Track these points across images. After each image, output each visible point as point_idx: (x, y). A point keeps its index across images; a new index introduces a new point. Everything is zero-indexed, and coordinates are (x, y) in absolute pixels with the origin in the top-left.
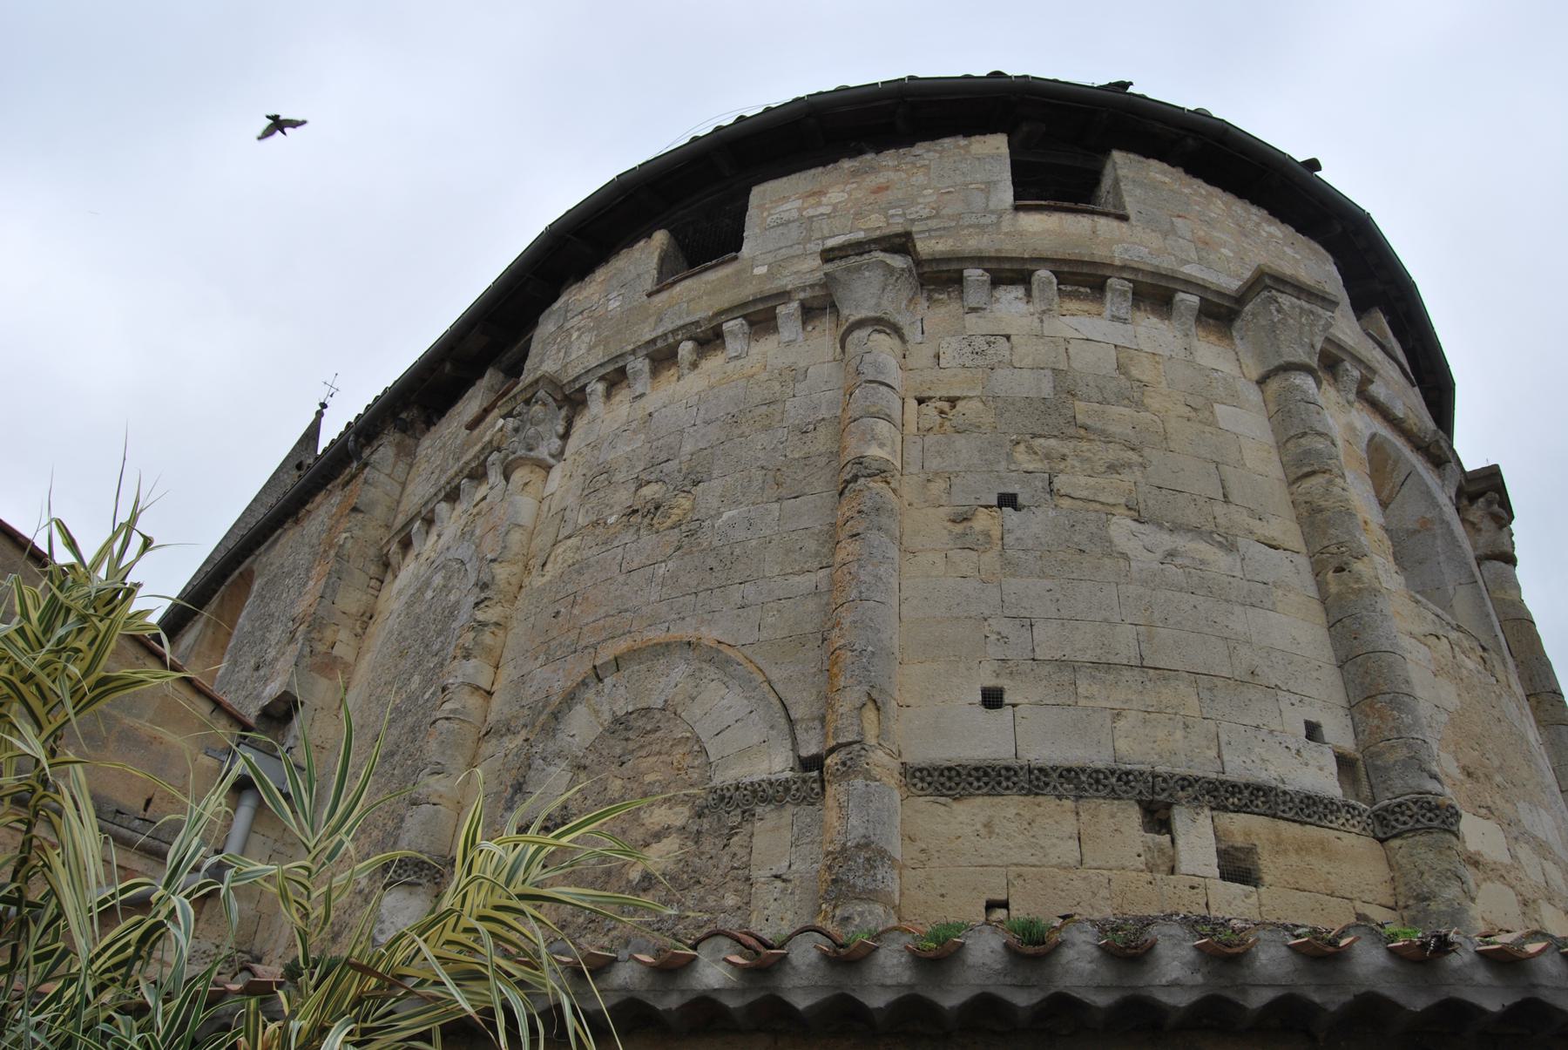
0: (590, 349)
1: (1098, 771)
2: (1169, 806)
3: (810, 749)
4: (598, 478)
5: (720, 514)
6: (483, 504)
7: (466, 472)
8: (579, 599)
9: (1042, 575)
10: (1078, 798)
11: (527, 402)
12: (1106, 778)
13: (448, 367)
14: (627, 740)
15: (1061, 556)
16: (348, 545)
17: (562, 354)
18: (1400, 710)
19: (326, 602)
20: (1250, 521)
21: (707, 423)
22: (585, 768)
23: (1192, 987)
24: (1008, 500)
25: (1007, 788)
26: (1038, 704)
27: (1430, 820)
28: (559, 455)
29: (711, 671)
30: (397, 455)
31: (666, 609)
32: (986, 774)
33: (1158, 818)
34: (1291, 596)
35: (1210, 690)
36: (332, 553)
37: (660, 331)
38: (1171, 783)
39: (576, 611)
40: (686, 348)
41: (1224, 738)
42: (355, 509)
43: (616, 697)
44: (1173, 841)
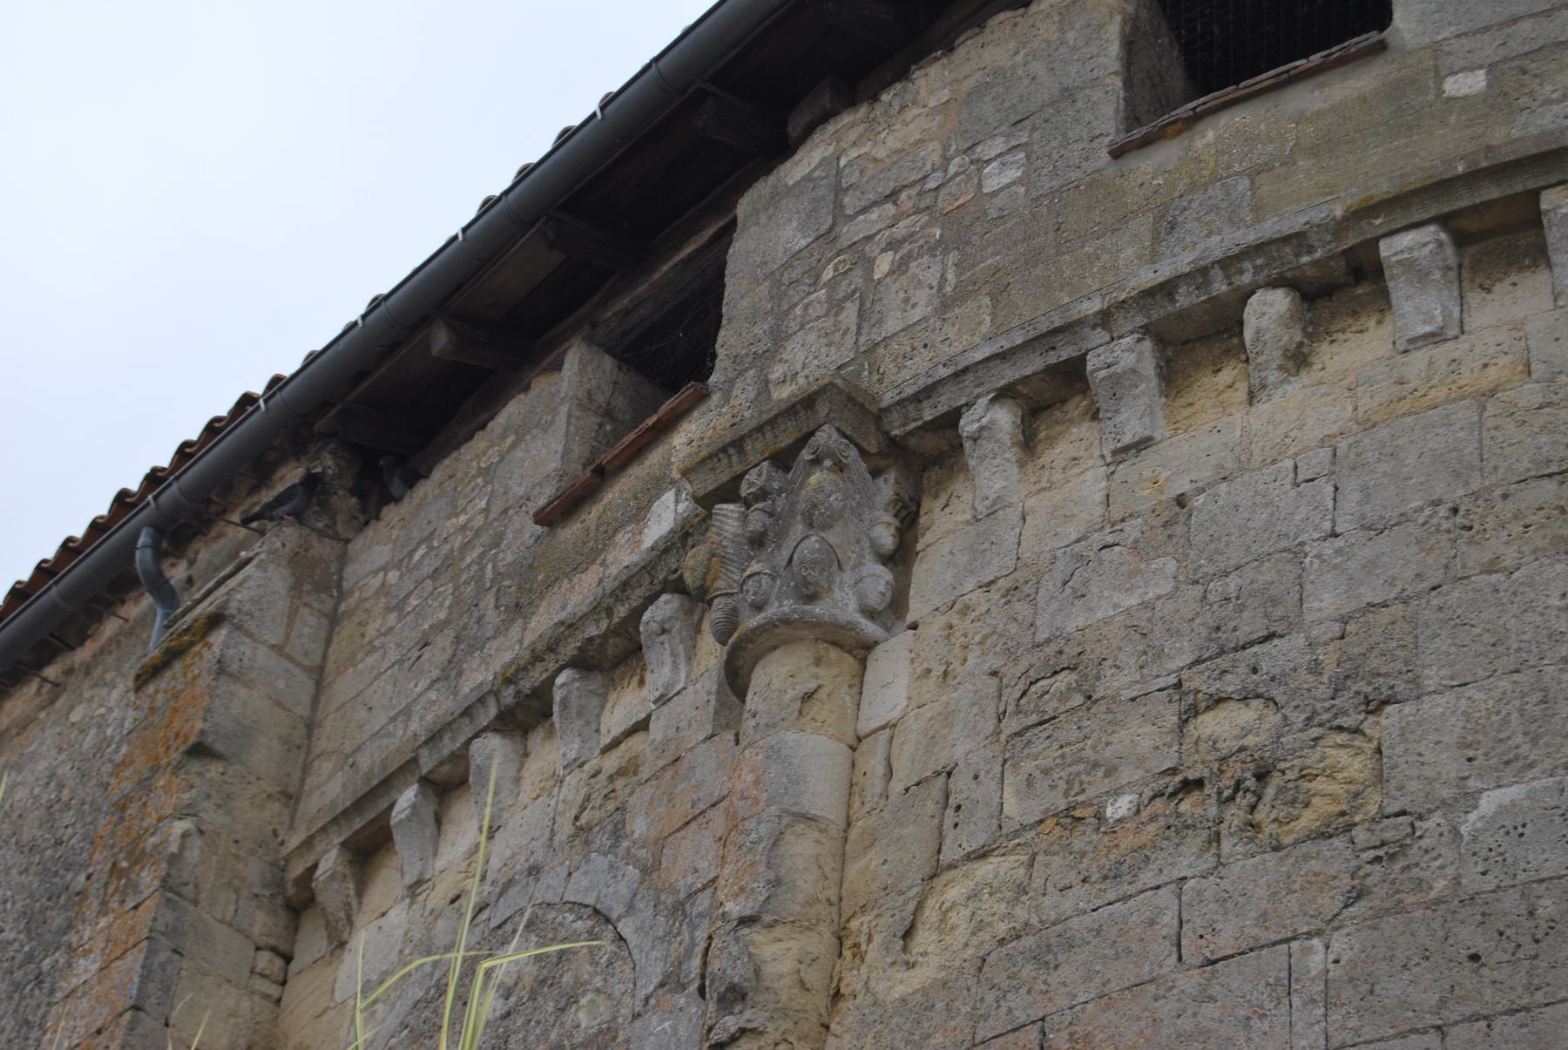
0: (945, 305)
4: (1047, 689)
5: (1470, 799)
6: (636, 743)
7: (569, 649)
11: (783, 460)
13: (441, 339)
16: (193, 854)
17: (850, 315)
19: (149, 1022)
21: (1374, 529)
28: (895, 607)
30: (296, 589)
36: (148, 878)
37: (1184, 261)
40: (1269, 311)
42: (200, 751)
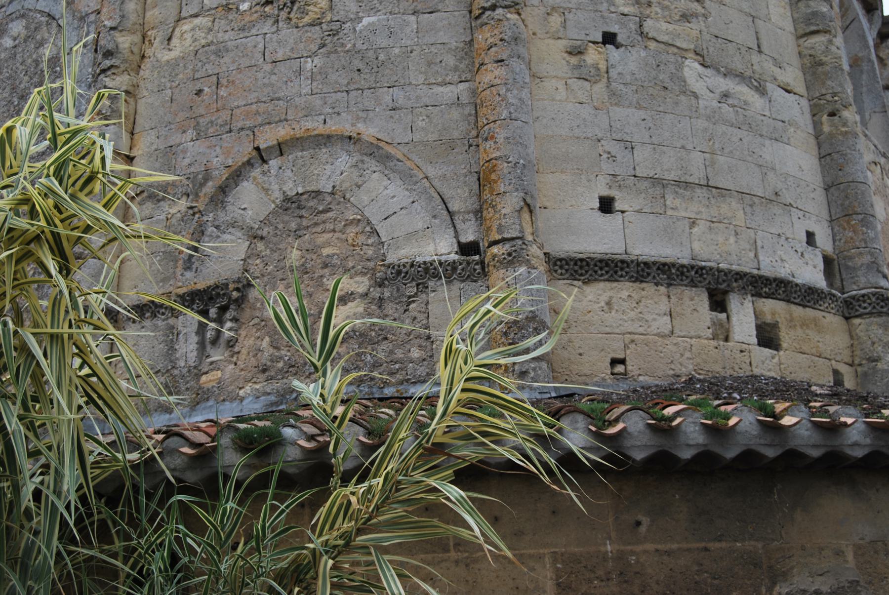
1: (683, 266)
2: (725, 293)
3: (468, 237)
5: (360, 20)
8: (224, 81)
9: (639, 107)
10: (669, 285)
12: (688, 271)
14: (301, 217)
15: (651, 91)
18: (868, 228)
20: (774, 68)
22: (262, 238)
23: (865, 446)
24: (609, 39)
25: (621, 276)
26: (639, 211)
27: (882, 307)
29: (372, 164)
31: (319, 102)
32: (607, 265)
33: (718, 304)
34: (799, 132)
35: (751, 206)
38: (730, 276)
39: (223, 92)
41: (759, 243)
43: (283, 178)
44: (728, 317)
